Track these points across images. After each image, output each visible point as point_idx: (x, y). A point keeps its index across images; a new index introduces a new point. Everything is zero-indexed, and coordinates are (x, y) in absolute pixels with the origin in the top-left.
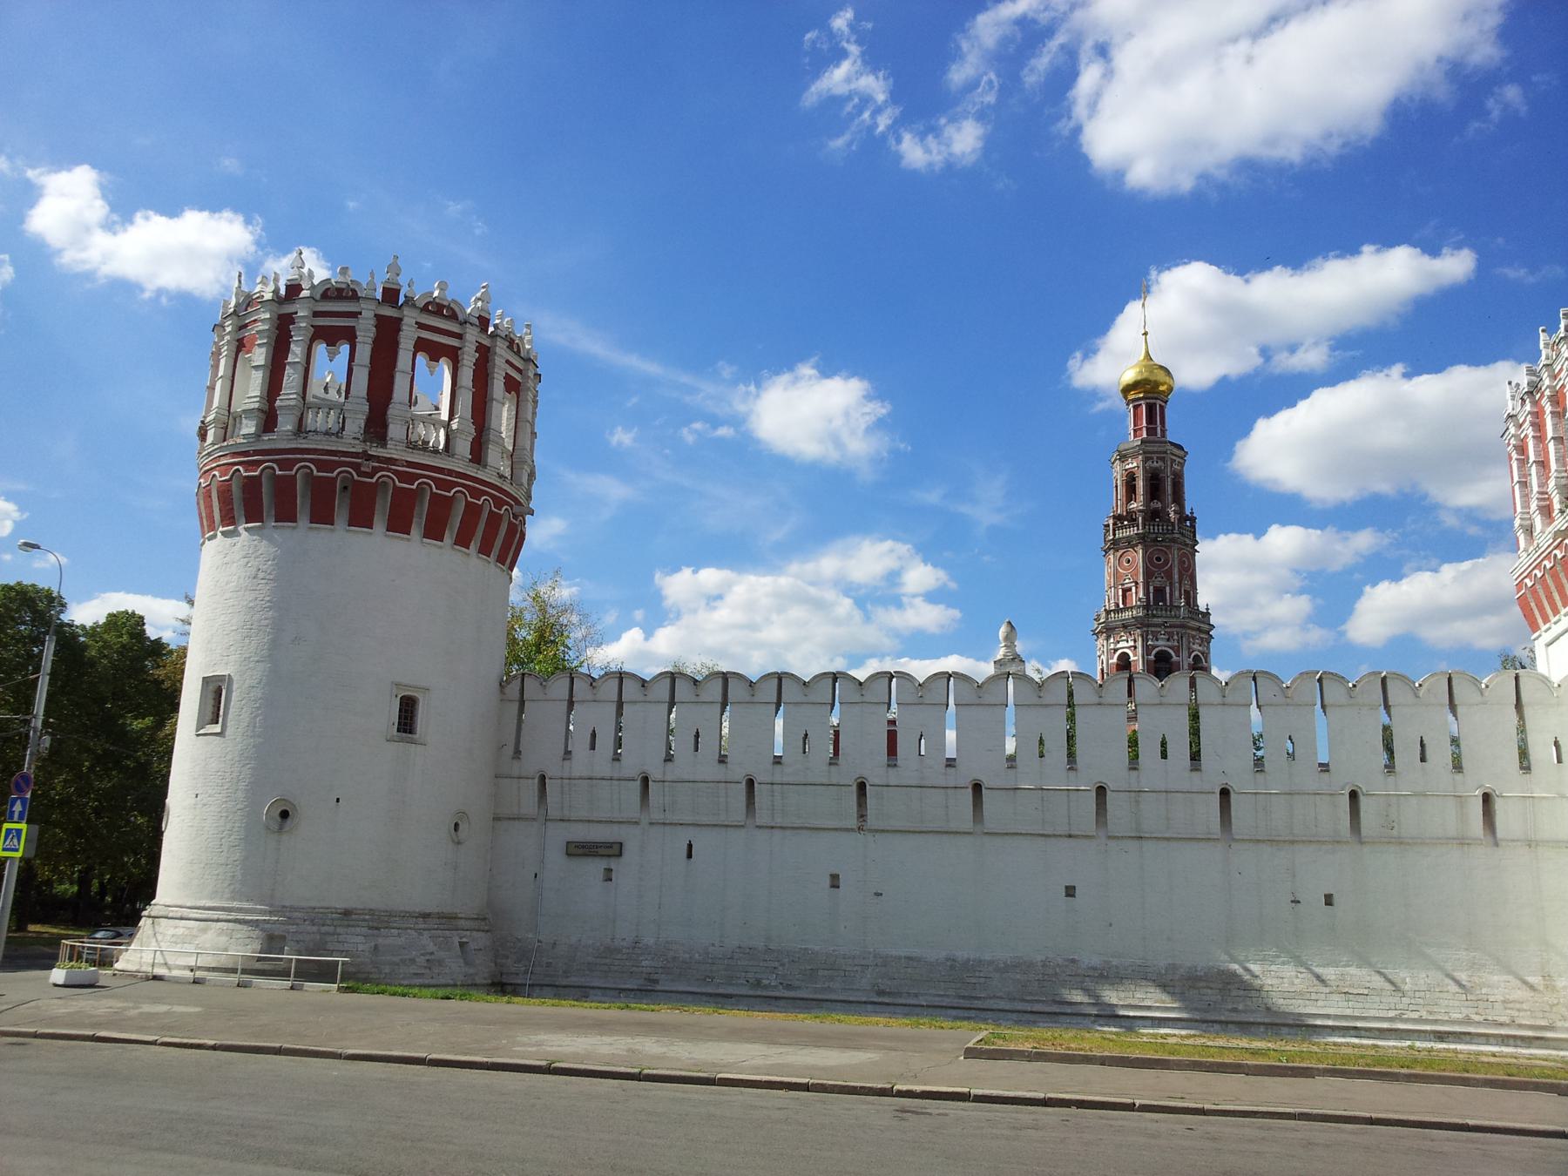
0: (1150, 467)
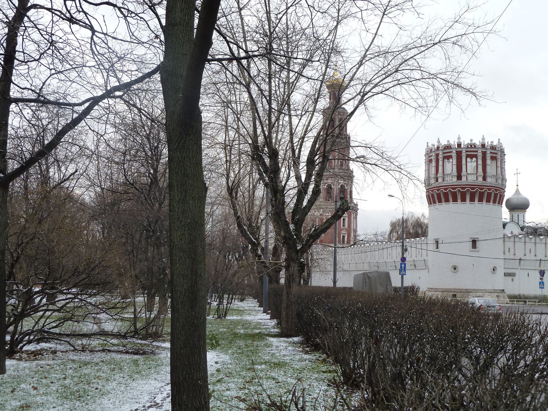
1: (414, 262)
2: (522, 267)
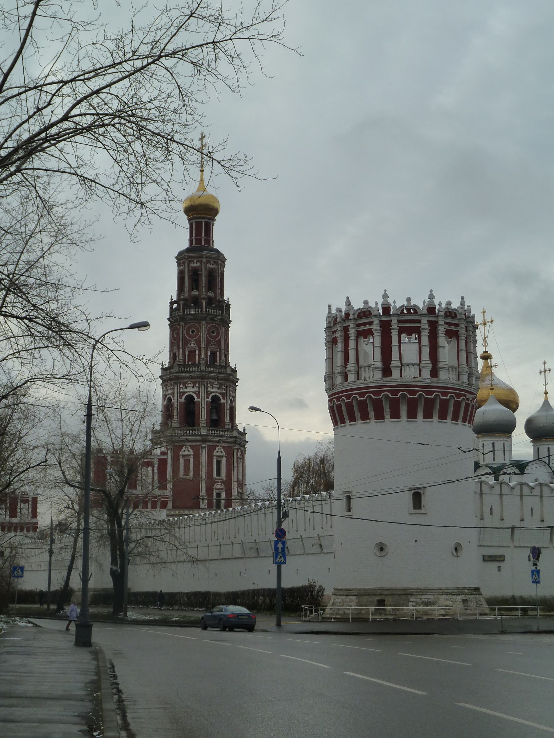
0: (209, 268)
1: (319, 539)
2: (517, 544)
